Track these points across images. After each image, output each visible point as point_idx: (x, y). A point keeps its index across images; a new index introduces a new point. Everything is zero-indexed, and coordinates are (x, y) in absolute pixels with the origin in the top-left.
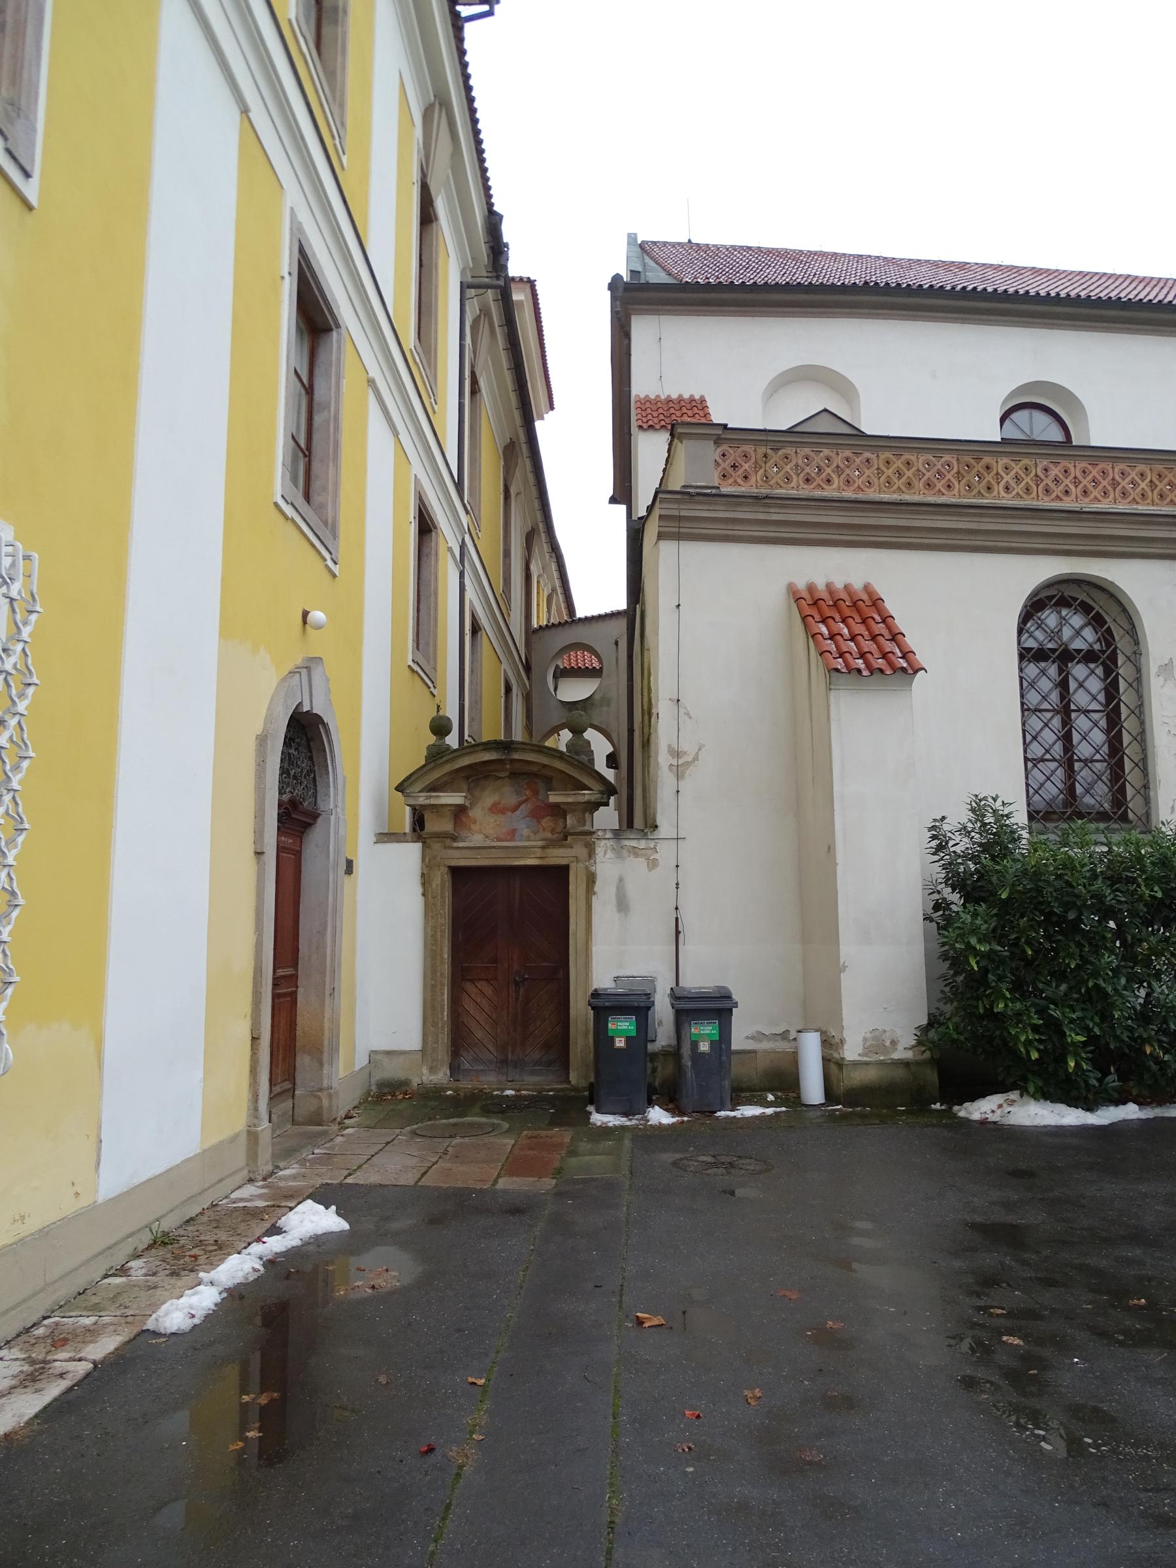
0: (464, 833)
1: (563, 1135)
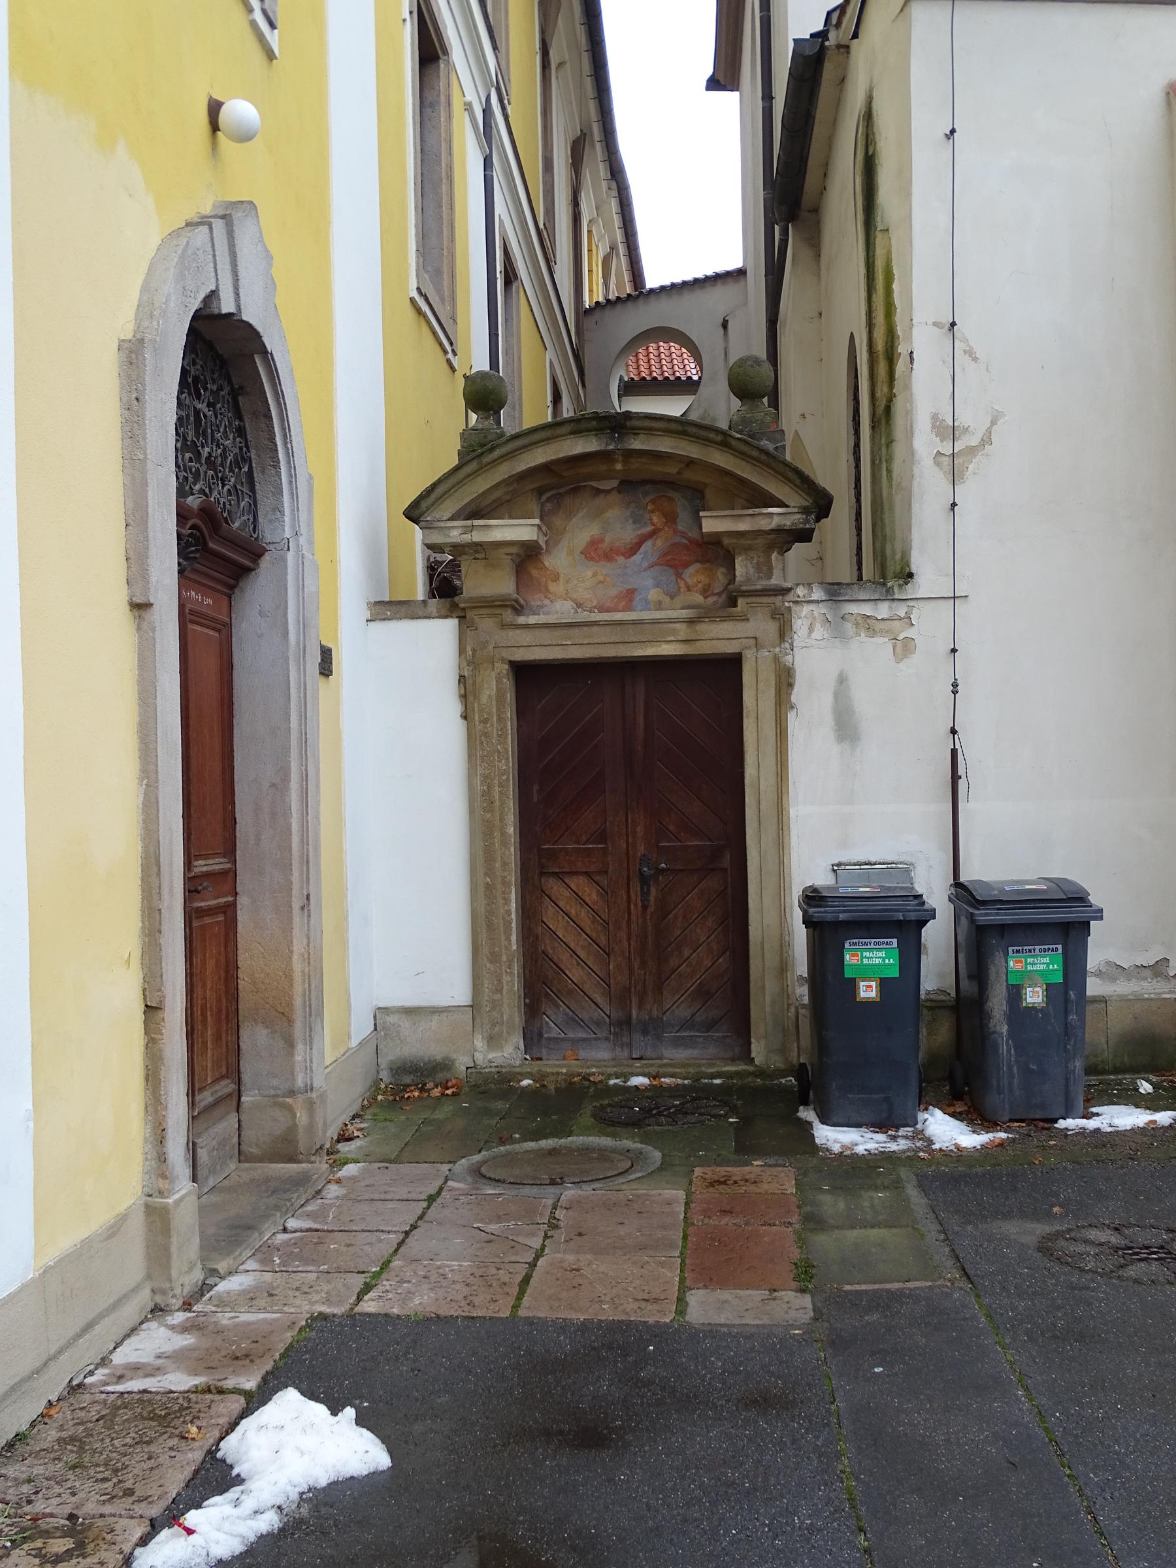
0: (535, 600)
1: (776, 1178)
